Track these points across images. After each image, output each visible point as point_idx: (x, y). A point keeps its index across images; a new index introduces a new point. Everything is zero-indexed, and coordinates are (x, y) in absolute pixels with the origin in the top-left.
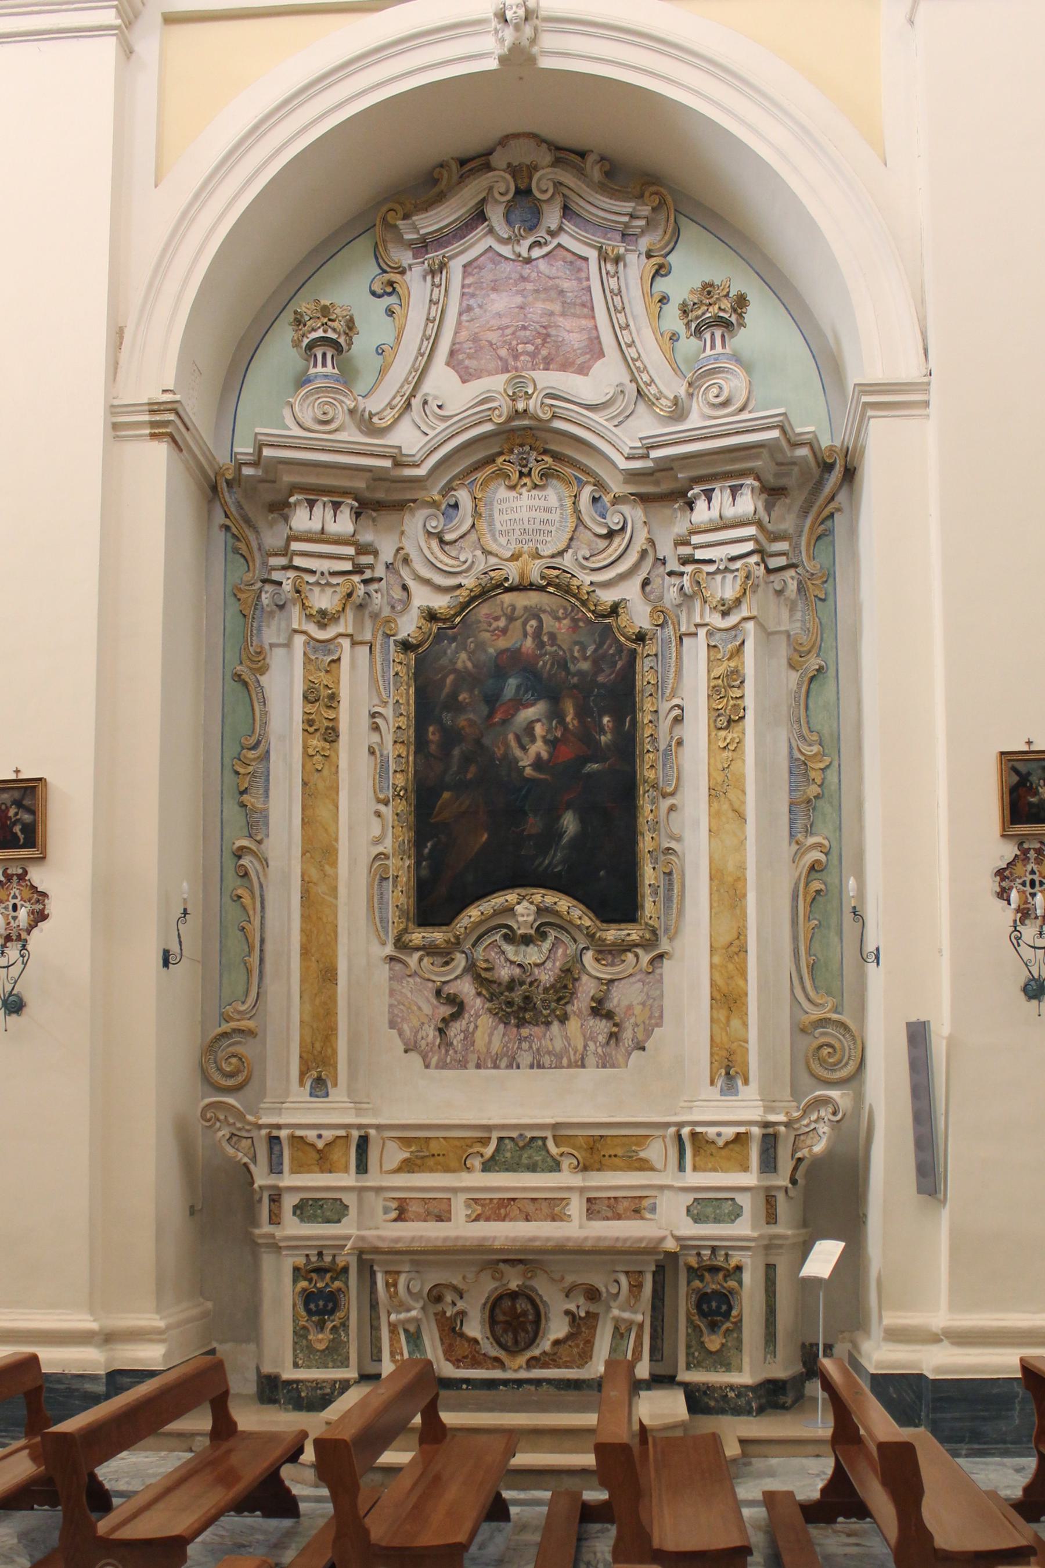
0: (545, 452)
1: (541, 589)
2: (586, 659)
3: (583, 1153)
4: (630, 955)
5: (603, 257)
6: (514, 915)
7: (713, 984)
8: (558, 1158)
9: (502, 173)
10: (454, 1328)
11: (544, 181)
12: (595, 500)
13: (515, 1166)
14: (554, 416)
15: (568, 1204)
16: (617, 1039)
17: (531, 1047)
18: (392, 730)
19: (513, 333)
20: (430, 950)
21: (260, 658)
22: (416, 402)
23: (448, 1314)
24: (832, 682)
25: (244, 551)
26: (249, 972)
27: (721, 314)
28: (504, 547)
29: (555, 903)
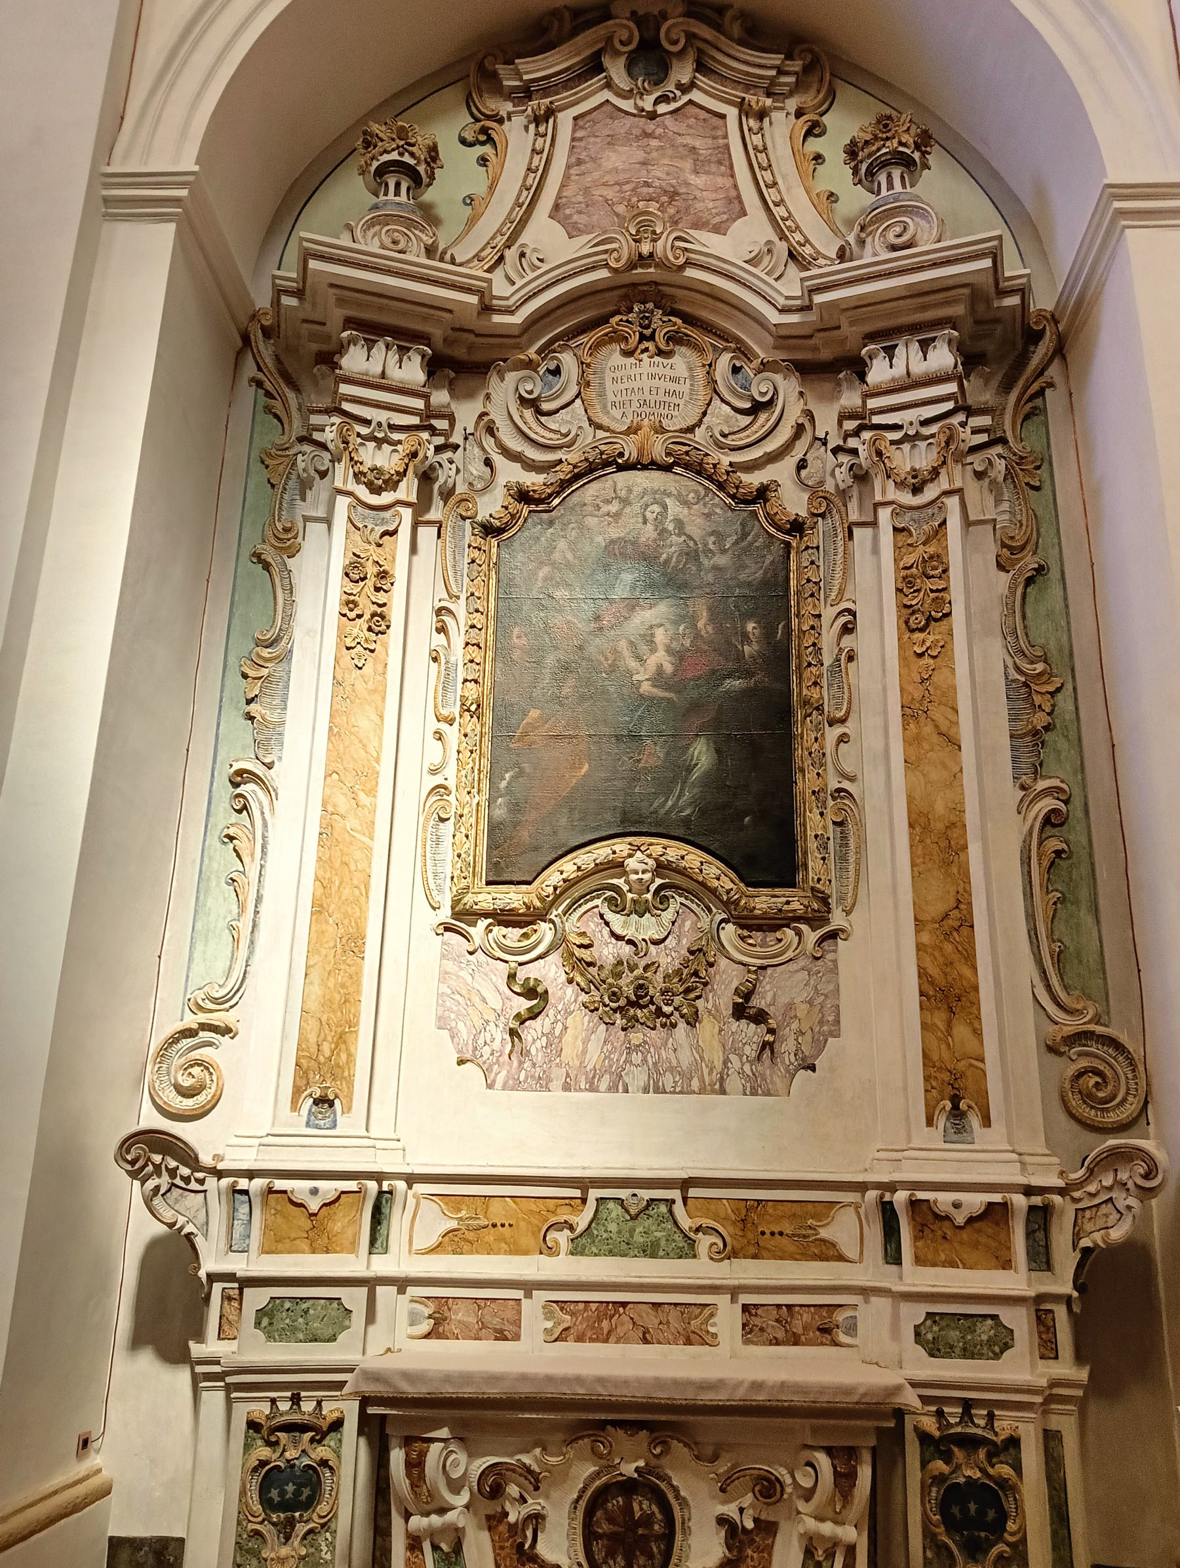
0: (674, 313)
1: (667, 468)
2: (724, 551)
3: (731, 1229)
4: (790, 933)
5: (744, 109)
6: (625, 873)
7: (922, 973)
8: (692, 1235)
9: (625, 22)
10: (522, 1544)
11: (675, 30)
12: (736, 370)
13: (624, 1246)
14: (689, 263)
15: (712, 1315)
16: (772, 1052)
17: (645, 1060)
18: (463, 630)
19: (633, 190)
20: (504, 918)
21: (290, 536)
22: (511, 254)
23: (512, 1518)
24: (1056, 590)
25: (280, 410)
26: (236, 941)
27: (901, 149)
28: (617, 420)
29: (683, 858)
